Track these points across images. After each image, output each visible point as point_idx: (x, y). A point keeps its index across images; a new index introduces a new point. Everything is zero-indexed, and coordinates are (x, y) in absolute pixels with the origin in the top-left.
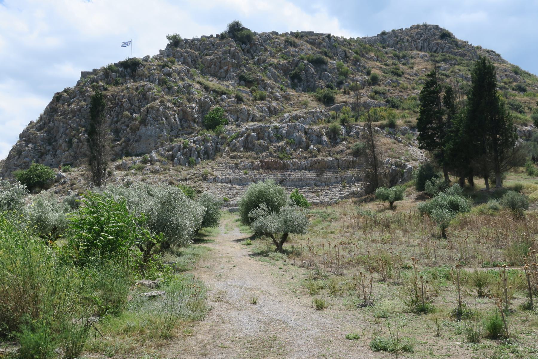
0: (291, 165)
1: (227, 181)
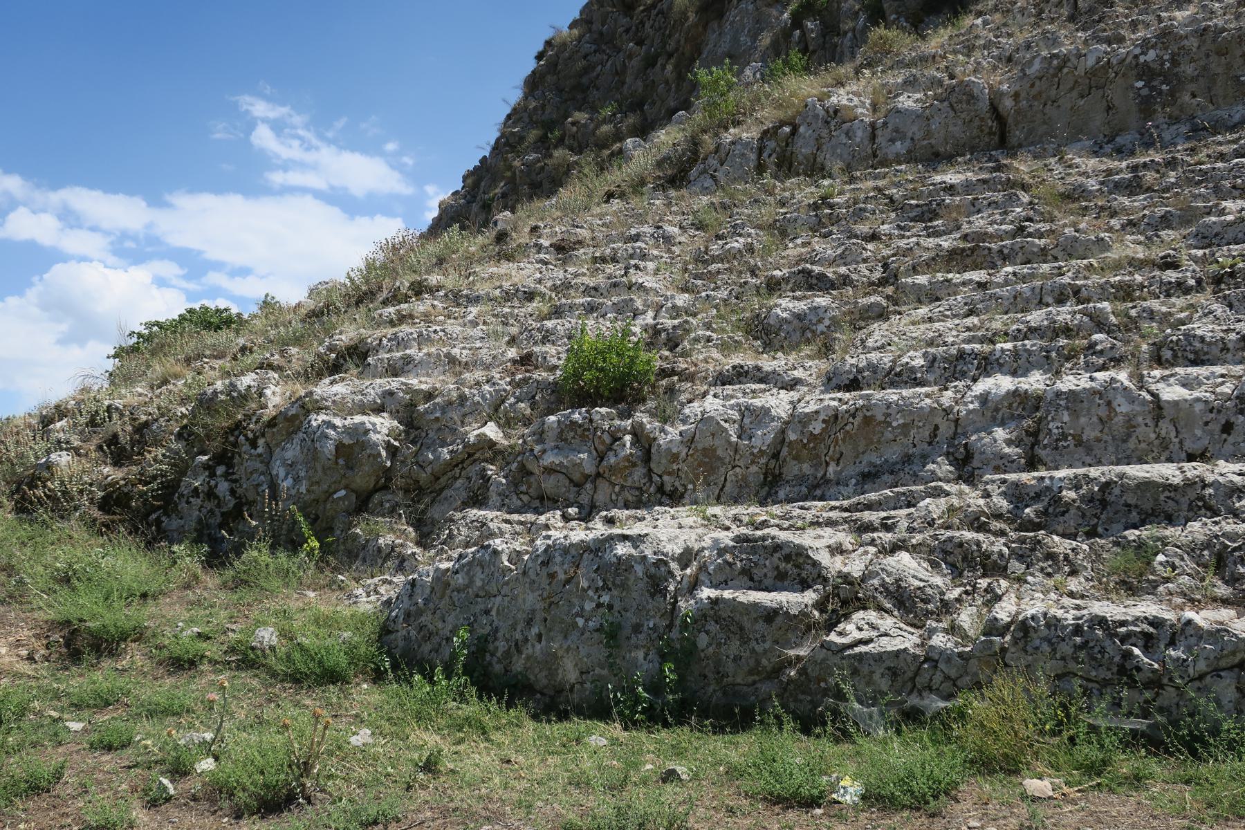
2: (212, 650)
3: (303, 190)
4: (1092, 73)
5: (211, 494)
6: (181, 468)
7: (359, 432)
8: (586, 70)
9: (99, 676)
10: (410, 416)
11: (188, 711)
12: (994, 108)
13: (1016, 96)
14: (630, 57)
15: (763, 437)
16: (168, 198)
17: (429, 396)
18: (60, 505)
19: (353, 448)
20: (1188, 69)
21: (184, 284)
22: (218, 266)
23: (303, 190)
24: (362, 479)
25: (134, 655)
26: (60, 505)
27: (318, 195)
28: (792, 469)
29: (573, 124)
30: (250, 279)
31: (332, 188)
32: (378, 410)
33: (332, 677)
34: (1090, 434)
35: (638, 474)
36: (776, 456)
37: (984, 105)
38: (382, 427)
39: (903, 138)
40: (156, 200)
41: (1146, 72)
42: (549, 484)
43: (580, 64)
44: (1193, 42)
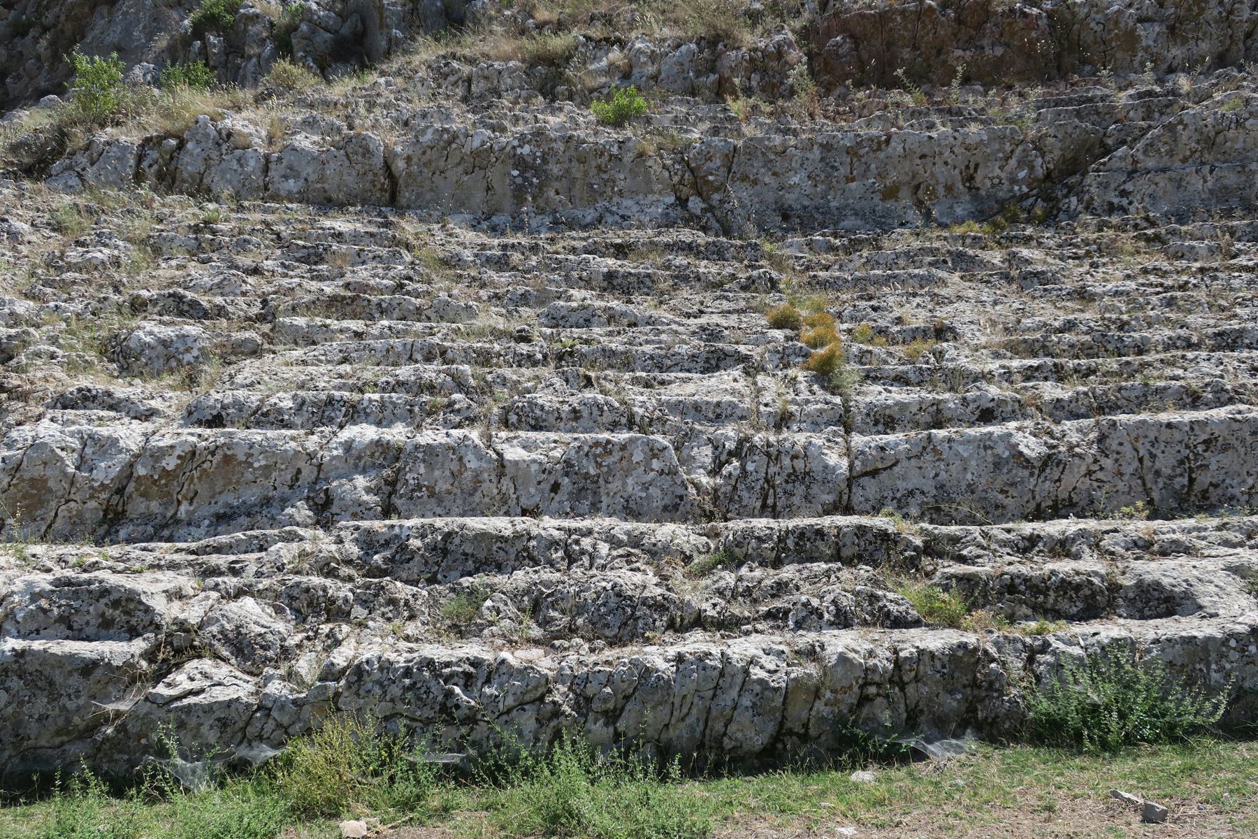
1: (340, 177)
4: (476, 154)
13: (409, 159)
20: (555, 169)
28: (138, 506)
34: (442, 486)
36: (120, 491)
39: (297, 176)
41: (521, 163)
44: (560, 146)
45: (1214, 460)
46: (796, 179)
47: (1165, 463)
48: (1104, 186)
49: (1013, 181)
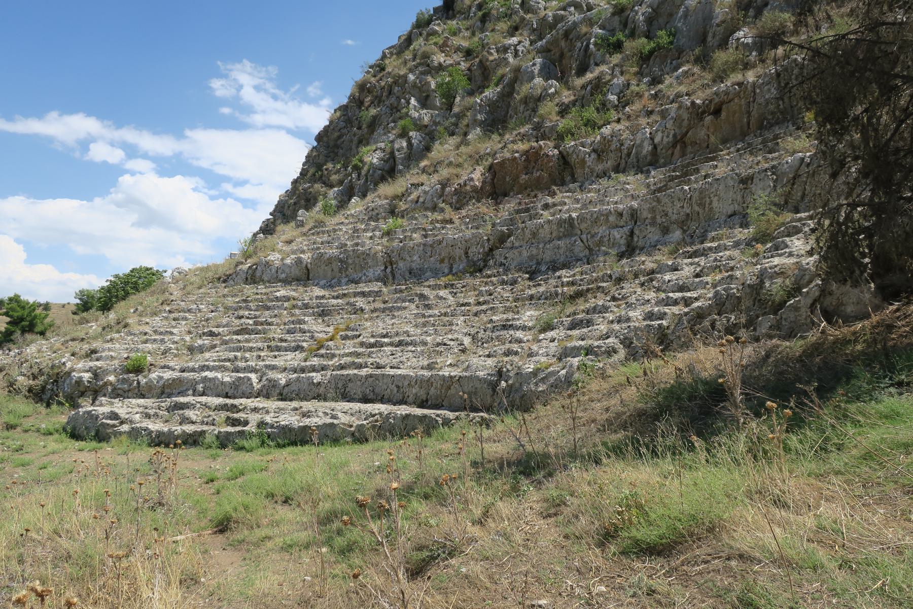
0: (590, 160)
2: (32, 428)
3: (279, 128)
4: (328, 259)
5: (52, 390)
6: (46, 383)
7: (81, 378)
8: (339, 137)
9: (11, 433)
10: (96, 375)
11: (815, 569)
12: (306, 266)
14: (355, 135)
15: (161, 383)
16: (188, 133)
17: (100, 368)
18: (18, 391)
19: (79, 382)
20: (350, 261)
21: (206, 190)
22: (226, 179)
23: (279, 128)
24: (82, 389)
25: (19, 429)
26: (18, 391)
27: (289, 131)
28: (167, 391)
29: (326, 169)
30: (248, 186)
31: (297, 127)
32: (87, 371)
33: (51, 434)
35: (136, 391)
37: (304, 266)
38: (87, 376)
40: (179, 135)
41: (341, 261)
42: (119, 392)
43: (336, 134)
44: (351, 253)
45: (350, 385)
46: (415, 258)
47: (340, 385)
48: (501, 255)
49: (479, 253)
